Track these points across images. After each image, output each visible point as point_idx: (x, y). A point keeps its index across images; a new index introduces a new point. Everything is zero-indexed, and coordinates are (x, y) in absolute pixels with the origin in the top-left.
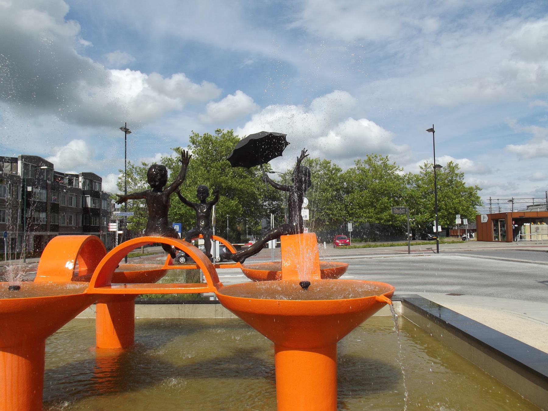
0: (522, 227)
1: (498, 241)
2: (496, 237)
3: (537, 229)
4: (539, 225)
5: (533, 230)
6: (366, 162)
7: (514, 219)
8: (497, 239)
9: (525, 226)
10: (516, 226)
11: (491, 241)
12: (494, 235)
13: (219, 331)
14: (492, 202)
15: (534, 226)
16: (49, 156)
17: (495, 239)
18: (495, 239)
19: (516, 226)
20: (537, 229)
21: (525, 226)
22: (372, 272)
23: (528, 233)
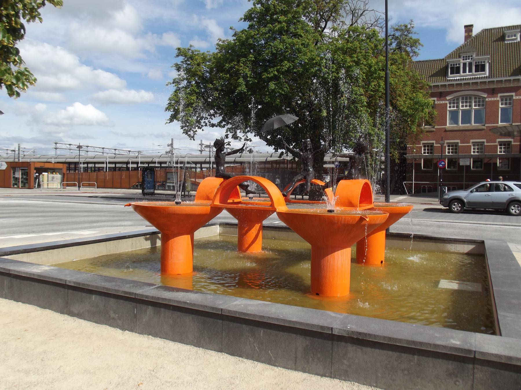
0: (41, 176)
1: (18, 187)
2: (14, 184)
3: (53, 178)
4: (54, 175)
5: (50, 179)
6: (248, 186)
7: (36, 169)
8: (16, 186)
9: (43, 175)
10: (37, 174)
11: (9, 187)
12: (13, 182)
13: (415, 258)
14: (117, 172)
15: (51, 175)
16: (141, 220)
17: (13, 186)
18: (13, 186)
19: (37, 174)
20: (53, 178)
21: (43, 175)
22: (10, 215)
23: (45, 181)
